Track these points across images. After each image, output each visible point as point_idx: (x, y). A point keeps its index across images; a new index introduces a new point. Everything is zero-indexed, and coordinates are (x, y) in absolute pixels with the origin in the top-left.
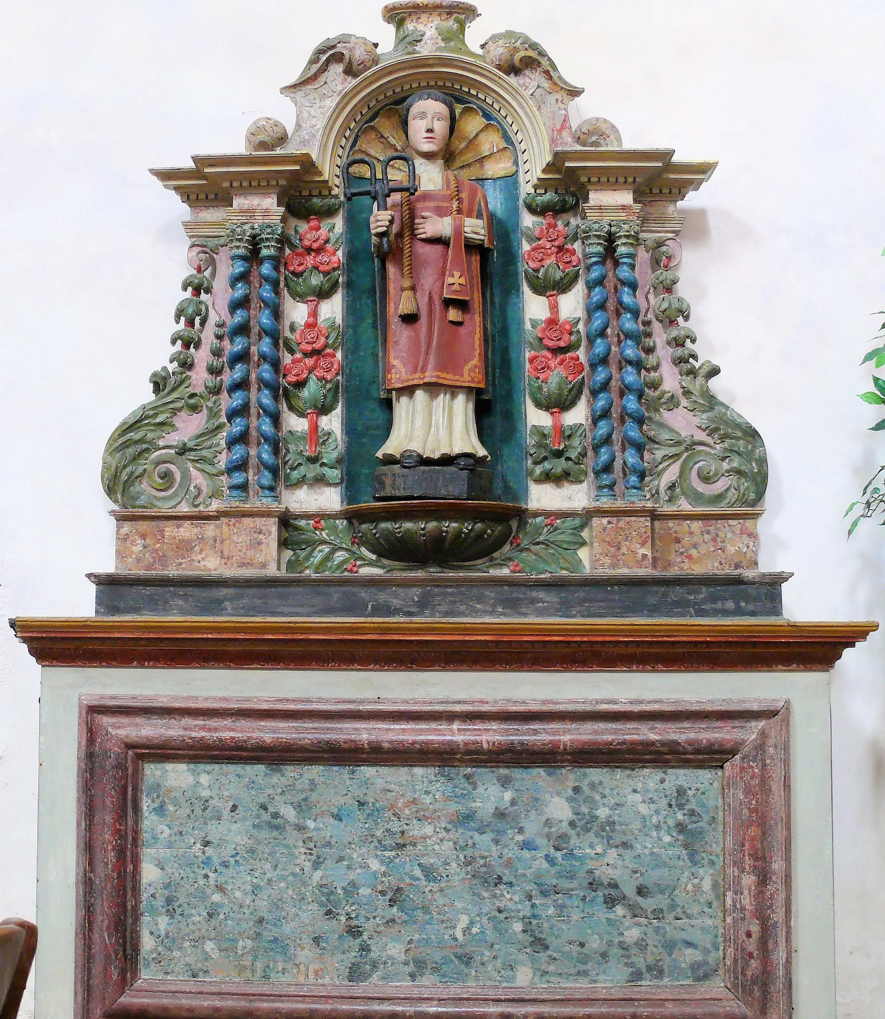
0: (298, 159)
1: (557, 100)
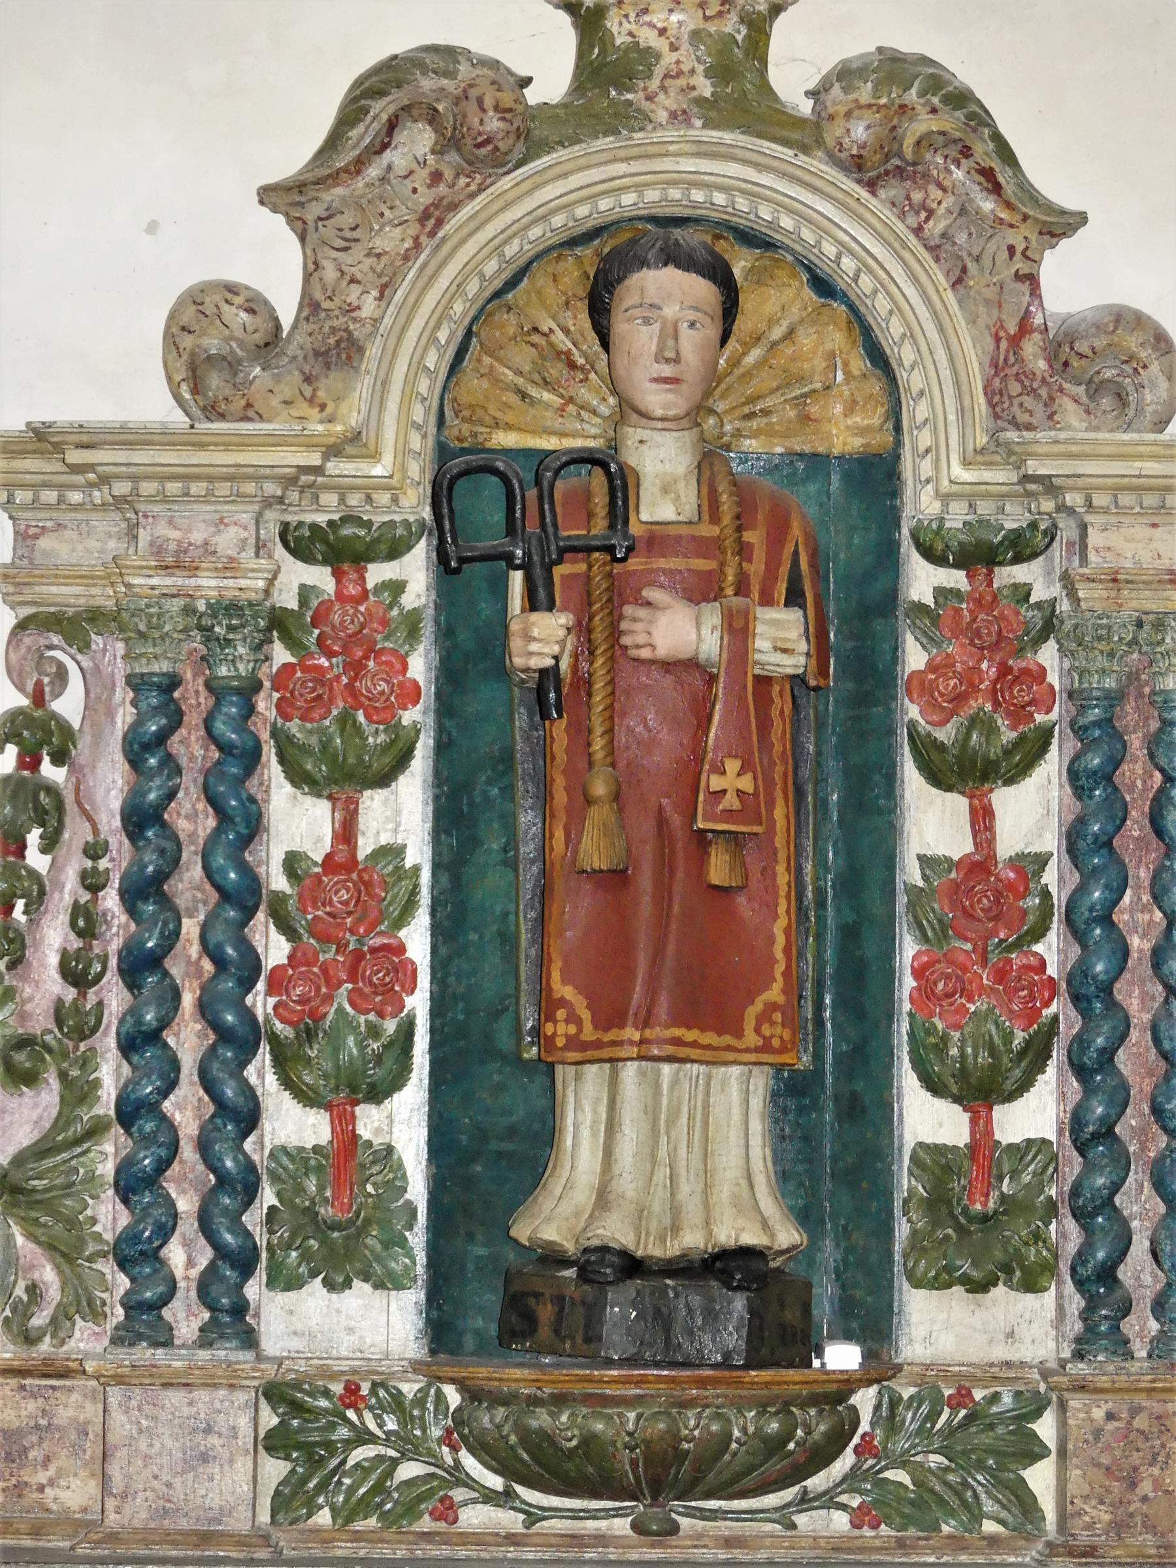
0: (316, 440)
1: (1011, 249)
